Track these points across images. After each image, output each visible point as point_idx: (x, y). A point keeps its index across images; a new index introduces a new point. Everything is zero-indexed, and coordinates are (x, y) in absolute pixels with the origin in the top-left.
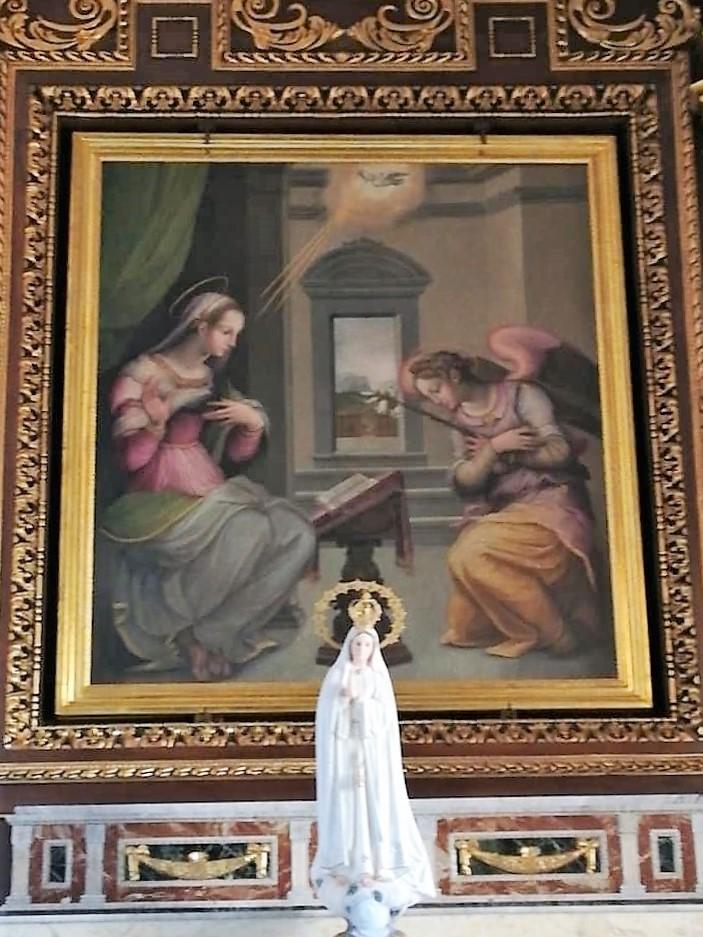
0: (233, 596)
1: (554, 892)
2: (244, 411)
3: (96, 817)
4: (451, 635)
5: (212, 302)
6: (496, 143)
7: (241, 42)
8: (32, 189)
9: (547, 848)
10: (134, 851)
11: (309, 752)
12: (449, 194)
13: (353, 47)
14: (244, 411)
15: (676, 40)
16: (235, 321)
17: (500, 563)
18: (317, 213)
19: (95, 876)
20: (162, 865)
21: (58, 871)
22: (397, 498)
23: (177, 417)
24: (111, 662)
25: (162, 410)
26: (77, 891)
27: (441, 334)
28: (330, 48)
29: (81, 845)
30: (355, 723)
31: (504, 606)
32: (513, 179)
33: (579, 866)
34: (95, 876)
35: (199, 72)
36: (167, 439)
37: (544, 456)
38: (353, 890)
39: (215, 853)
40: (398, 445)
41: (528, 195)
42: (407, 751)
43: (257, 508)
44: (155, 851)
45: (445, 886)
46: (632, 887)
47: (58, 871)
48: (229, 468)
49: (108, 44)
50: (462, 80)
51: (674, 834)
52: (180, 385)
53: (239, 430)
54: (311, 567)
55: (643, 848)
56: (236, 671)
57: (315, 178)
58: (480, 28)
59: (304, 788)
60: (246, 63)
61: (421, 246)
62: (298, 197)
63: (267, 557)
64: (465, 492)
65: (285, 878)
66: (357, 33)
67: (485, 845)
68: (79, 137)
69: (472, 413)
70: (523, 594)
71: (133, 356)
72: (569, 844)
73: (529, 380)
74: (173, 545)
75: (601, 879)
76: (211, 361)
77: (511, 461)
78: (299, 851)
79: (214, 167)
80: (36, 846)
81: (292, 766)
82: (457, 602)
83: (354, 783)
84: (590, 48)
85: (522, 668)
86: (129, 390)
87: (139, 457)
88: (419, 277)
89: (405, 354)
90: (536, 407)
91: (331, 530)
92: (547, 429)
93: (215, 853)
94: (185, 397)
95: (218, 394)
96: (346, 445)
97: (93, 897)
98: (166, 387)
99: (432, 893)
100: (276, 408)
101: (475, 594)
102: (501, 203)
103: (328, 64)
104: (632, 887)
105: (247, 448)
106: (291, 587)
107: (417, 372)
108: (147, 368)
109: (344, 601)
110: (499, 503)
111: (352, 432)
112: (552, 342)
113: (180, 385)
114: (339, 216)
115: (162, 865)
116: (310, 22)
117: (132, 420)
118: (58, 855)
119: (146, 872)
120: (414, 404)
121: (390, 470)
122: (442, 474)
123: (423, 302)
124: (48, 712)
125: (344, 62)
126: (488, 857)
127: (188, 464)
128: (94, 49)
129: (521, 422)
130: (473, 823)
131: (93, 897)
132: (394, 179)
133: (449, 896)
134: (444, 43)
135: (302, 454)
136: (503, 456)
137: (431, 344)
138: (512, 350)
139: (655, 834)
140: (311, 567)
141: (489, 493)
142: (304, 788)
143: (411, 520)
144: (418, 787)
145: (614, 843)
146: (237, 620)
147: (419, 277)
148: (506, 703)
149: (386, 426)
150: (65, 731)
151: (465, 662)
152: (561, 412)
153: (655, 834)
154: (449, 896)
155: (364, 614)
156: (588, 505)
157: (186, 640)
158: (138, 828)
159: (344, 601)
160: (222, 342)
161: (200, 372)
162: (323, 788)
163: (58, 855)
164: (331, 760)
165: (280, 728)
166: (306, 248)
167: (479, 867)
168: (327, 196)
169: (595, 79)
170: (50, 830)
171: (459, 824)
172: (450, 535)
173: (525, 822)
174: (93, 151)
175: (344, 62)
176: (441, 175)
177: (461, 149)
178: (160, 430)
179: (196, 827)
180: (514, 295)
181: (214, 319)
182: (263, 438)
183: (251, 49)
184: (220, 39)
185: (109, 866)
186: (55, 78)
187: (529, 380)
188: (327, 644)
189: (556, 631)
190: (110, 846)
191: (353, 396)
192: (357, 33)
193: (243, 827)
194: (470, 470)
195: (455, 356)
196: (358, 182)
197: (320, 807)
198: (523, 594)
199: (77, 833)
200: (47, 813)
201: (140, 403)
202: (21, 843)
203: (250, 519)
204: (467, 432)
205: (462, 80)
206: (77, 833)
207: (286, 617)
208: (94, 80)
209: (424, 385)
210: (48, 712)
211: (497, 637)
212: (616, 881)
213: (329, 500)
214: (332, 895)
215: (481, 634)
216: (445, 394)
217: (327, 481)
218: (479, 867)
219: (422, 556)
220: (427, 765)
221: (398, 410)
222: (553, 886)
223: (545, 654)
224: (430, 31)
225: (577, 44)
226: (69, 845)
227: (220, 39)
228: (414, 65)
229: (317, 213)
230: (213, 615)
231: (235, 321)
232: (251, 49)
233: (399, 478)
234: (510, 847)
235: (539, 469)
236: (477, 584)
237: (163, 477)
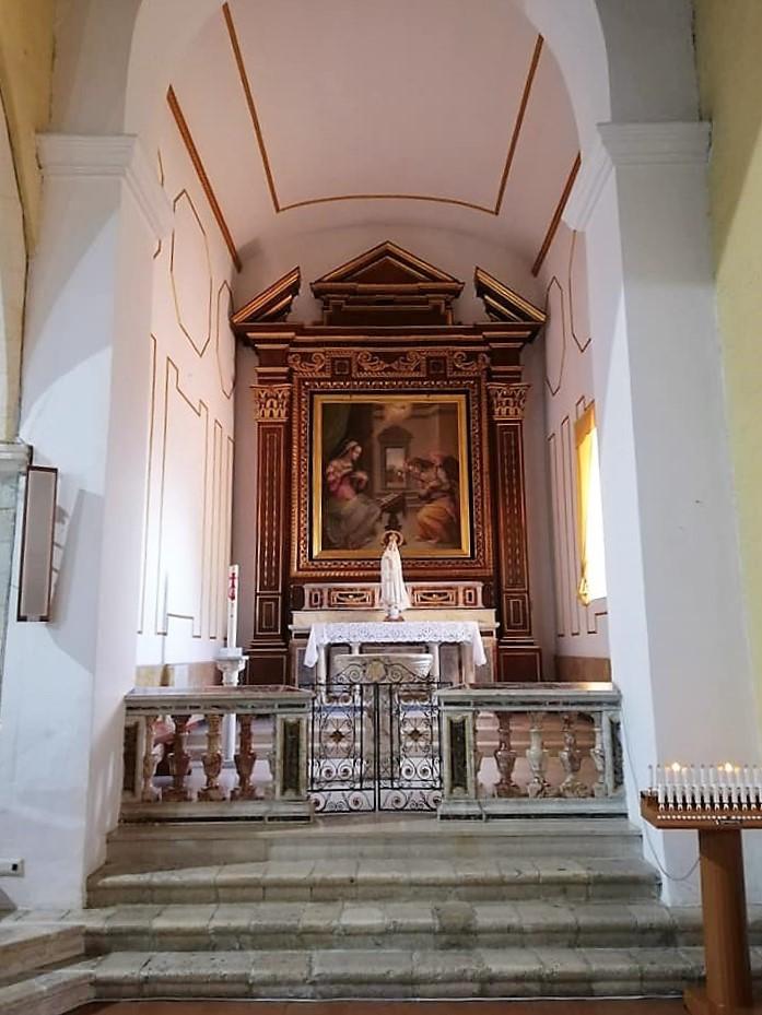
0: (359, 527)
1: (441, 607)
2: (362, 475)
3: (326, 586)
4: (417, 537)
5: (353, 444)
6: (432, 397)
7: (360, 369)
8: (303, 412)
9: (440, 595)
10: (336, 595)
11: (379, 569)
12: (418, 412)
13: (391, 370)
14: (362, 475)
15: (484, 367)
16: (359, 449)
17: (433, 519)
18: (382, 418)
19: (325, 601)
20: (342, 599)
21: (316, 600)
22: (404, 500)
23: (345, 476)
24: (326, 545)
25: (339, 475)
26: (321, 605)
27: (416, 453)
28: (386, 370)
29: (322, 594)
30: (391, 566)
31: (432, 530)
32: (437, 407)
33: (448, 599)
34: (325, 601)
35: (349, 378)
36: (341, 484)
37: (443, 488)
38: (390, 606)
39: (355, 596)
40: (404, 485)
41: (440, 412)
42: (403, 569)
43: (365, 502)
44: (341, 595)
45: (414, 604)
46: (461, 605)
47: (316, 600)
48: (358, 491)
49: (323, 370)
50: (422, 379)
51: (473, 592)
52: (344, 468)
53: (361, 480)
54: (380, 518)
55: (464, 595)
56: (359, 548)
57: (381, 407)
58: (428, 364)
59: (378, 579)
60: (363, 375)
61: (408, 428)
62: (377, 413)
63: (368, 516)
64: (422, 498)
65: (373, 602)
66: (394, 366)
67: (424, 594)
68: (316, 396)
69: (424, 476)
70: (437, 526)
71: (331, 459)
72: (445, 594)
73: (440, 466)
74: (342, 513)
75: (454, 603)
76: (353, 461)
77: (434, 489)
78: (377, 596)
79: (353, 404)
80: (311, 595)
81: (375, 573)
82: (419, 529)
83: (390, 580)
84: (460, 370)
85: (436, 547)
86: (330, 469)
87: (333, 489)
88: (410, 437)
89: (406, 459)
90: (442, 474)
91: (385, 509)
92: (444, 480)
93: (355, 596)
94: (345, 471)
95: (355, 470)
96: (389, 485)
97: (325, 606)
98: (340, 468)
99: (410, 606)
100: (370, 473)
101: (424, 526)
102: (434, 414)
103: (385, 375)
104: (461, 605)
105: (362, 486)
106: (374, 524)
107: (409, 465)
108: (335, 463)
109: (388, 536)
110: (431, 501)
111: (391, 481)
112: (446, 455)
113: (344, 468)
114: (388, 418)
115: (342, 599)
116: (497, 621)
117: (332, 478)
118: (316, 596)
119: (338, 600)
120: (408, 472)
121: (401, 492)
122: (415, 493)
123: (412, 444)
124: (311, 558)
125: (390, 375)
126: (424, 597)
127: (347, 490)
128: (320, 371)
129: (437, 478)
130: (421, 588)
131: (325, 606)
132: (403, 407)
133: (415, 607)
134: (417, 369)
135: (378, 488)
136: (432, 488)
137: (413, 455)
138: (435, 457)
139: (467, 591)
140: (380, 518)
141: (428, 498)
142: (378, 579)
143: (253, 746)
144: (406, 579)
145: (457, 594)
146: (361, 533)
147: (410, 437)
148: (428, 906)
149: (401, 479)
150: (315, 563)
151: (422, 544)
152: (448, 476)
153: (467, 591)
154: (415, 607)
155: (393, 538)
156: (456, 503)
157: (346, 538)
158: (337, 589)
159: (388, 536)
160: (355, 455)
161: (350, 464)
162: (383, 580)
163: (316, 596)
164: (385, 573)
165: (372, 563)
166: (379, 428)
167: (422, 600)
168: (385, 413)
169: (461, 379)
170: (314, 590)
171: (418, 589)
172: (418, 510)
173: (435, 588)
174: (320, 400)
175: (390, 375)
176: (416, 406)
177: (422, 399)
178: (338, 481)
179: (351, 590)
180: (436, 441)
181: (353, 448)
182: (367, 483)
183: (364, 371)
184: (354, 367)
185: (329, 599)
186: (309, 380)
187: (440, 466)
188: (227, 788)
189: (445, 535)
190: (329, 593)
191: (391, 471)
192: (394, 366)
193: (363, 589)
194: (423, 492)
195: (419, 459)
196: (394, 410)
197: (382, 584)
198: (437, 526)
199: (321, 590)
200: (312, 585)
201: (333, 473)
202: (307, 593)
203: (363, 505)
204: (423, 481)
205: (422, 379)
206: (321, 590)
207: (373, 533)
208: (319, 380)
209: (411, 468)
210: (311, 558)
211: (430, 539)
212: (457, 604)
213: (385, 500)
214: (385, 607)
215: (425, 537)
216: (417, 471)
217: (385, 495)
218: (422, 600)
219: (409, 515)
220: (408, 573)
221: (404, 475)
222: (441, 605)
223: (442, 543)
224: (414, 364)
225: (455, 369)
226: (319, 593)
227: (354, 367)
228: (409, 376)
229: (382, 418)
230: (355, 532)
231: (359, 449)
232: (364, 371)
233: (404, 494)
234: (430, 595)
235: (443, 491)
236: (425, 524)
237: (340, 493)
